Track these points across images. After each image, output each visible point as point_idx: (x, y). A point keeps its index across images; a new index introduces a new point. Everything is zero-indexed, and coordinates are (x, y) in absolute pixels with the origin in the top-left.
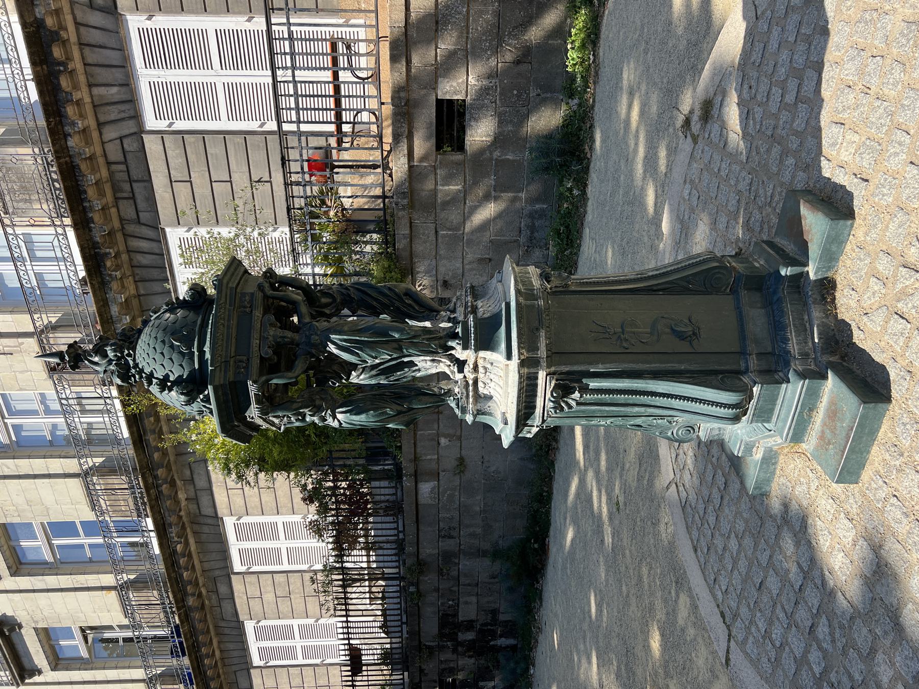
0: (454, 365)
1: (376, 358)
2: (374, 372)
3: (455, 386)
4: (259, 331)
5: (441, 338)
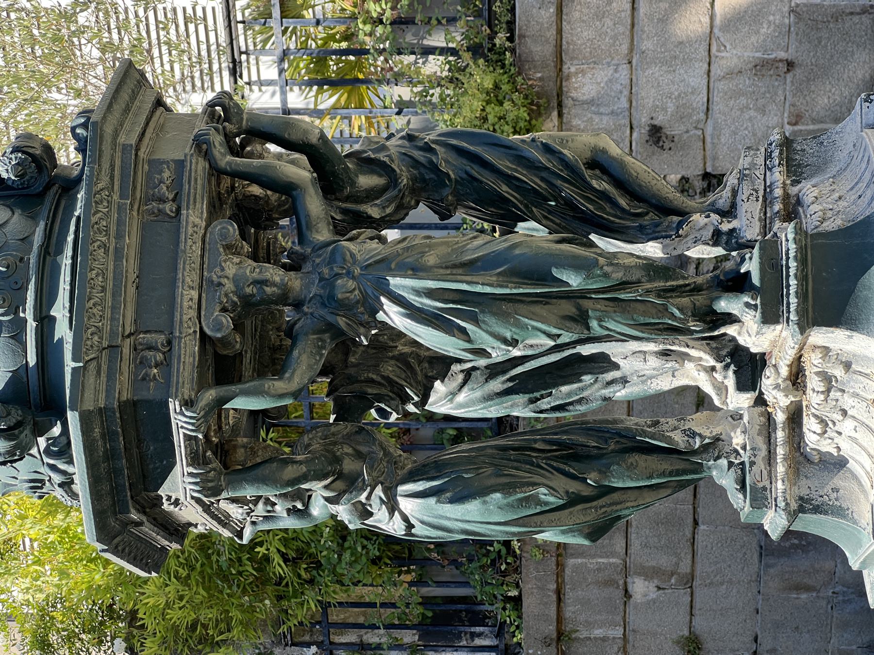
0: (727, 367)
1: (514, 343)
2: (497, 385)
3: (734, 428)
4: (197, 266)
5: (697, 289)
